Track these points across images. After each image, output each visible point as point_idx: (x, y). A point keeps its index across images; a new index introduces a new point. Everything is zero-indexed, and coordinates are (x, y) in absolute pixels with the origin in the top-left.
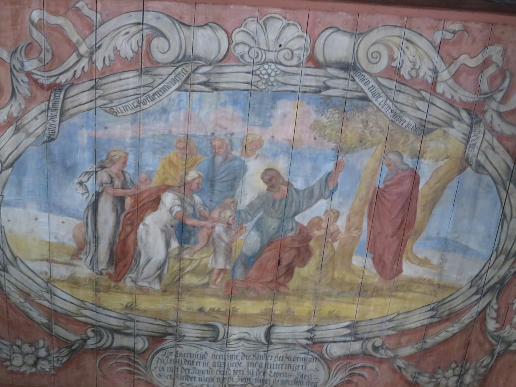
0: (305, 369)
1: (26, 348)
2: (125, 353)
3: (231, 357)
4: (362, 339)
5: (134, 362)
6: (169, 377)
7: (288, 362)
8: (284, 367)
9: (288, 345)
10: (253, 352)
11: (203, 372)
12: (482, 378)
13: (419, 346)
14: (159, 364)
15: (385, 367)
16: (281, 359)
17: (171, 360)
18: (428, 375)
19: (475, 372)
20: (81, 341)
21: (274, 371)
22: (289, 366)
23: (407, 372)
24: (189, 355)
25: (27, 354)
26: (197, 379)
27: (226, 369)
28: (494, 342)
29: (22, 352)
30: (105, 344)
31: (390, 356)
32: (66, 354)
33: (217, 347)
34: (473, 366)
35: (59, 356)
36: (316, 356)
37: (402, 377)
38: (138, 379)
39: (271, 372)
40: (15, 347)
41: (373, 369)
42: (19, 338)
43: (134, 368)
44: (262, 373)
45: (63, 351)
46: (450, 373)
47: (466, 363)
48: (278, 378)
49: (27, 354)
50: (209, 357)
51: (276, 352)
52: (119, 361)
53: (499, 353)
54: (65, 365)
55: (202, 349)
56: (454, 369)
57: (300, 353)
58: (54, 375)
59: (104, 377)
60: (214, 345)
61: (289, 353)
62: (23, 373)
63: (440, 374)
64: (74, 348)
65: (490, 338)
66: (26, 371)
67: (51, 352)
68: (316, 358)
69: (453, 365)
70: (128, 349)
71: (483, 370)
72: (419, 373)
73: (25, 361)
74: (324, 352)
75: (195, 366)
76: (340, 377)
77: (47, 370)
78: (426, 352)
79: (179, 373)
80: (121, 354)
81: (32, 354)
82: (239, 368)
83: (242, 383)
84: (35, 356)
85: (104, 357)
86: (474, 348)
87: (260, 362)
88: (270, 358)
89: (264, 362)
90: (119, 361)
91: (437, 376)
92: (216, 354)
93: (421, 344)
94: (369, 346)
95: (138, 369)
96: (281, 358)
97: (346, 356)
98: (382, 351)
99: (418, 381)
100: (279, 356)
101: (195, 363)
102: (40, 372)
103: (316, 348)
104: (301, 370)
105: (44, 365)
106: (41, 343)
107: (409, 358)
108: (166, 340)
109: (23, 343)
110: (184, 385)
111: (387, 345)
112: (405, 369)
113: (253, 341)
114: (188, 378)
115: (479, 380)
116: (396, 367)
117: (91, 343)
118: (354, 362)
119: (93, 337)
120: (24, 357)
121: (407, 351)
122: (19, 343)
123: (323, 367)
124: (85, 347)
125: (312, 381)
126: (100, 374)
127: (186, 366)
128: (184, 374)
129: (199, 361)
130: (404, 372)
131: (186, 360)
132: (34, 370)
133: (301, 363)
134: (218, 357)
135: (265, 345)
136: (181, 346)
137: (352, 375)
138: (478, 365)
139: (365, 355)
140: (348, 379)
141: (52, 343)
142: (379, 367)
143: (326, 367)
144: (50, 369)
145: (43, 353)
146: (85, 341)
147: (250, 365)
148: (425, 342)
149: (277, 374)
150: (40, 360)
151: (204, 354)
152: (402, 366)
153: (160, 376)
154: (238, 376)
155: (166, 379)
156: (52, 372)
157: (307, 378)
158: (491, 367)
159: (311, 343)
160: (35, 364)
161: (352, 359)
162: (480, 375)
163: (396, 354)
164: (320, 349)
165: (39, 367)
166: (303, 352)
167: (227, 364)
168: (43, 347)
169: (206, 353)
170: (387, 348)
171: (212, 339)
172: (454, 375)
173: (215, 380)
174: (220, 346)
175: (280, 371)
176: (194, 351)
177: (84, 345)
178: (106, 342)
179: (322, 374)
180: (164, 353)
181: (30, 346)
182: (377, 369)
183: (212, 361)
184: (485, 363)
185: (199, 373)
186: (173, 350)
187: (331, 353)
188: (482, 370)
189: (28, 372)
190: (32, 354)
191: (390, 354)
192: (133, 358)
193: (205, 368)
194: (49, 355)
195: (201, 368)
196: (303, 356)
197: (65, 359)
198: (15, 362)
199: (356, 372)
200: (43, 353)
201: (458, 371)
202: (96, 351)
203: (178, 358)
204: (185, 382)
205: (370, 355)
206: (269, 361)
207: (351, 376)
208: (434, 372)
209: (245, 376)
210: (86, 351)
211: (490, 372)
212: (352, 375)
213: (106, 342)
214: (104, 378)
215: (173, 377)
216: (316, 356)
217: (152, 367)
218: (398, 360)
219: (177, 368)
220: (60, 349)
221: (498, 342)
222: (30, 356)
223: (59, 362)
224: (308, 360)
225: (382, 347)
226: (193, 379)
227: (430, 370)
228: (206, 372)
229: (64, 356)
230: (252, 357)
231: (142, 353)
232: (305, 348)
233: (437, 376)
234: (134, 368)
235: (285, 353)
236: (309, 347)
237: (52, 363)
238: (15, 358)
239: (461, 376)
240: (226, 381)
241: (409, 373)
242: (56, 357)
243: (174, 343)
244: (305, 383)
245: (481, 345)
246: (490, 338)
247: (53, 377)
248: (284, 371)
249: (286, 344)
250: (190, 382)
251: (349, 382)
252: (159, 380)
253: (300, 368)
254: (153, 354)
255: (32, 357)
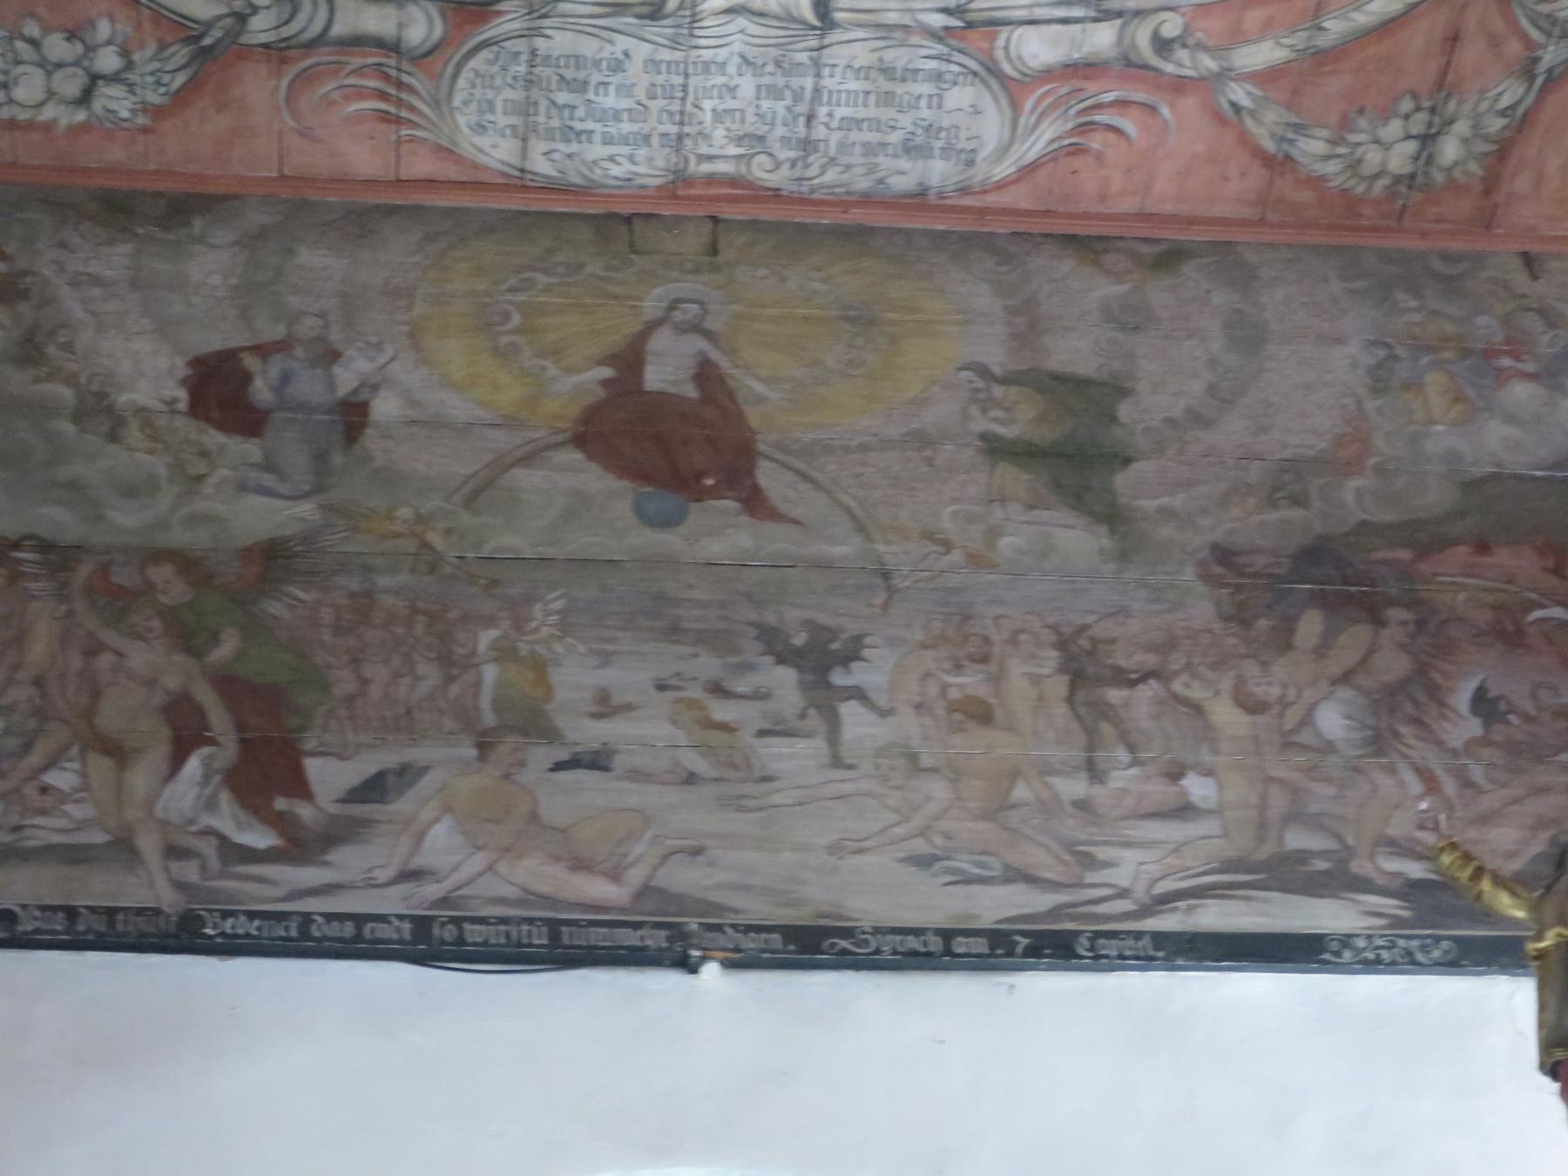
0: (940, 107)
1: (57, 47)
2: (371, 55)
3: (707, 65)
4: (1119, 14)
5: (400, 85)
6: (508, 131)
7: (886, 86)
8: (872, 99)
9: (886, 31)
10: (774, 52)
11: (617, 116)
12: (1495, 147)
13: (1299, 39)
14: (478, 92)
15: (1190, 103)
16: (862, 75)
17: (515, 78)
18: (1325, 133)
19: (1474, 127)
20: (229, 21)
21: (841, 112)
22: (887, 99)
23: (1259, 122)
24: (572, 61)
25: (60, 66)
26: (597, 138)
27: (689, 107)
28: (1535, 34)
29: (44, 58)
30: (303, 30)
31: (1209, 70)
32: (183, 61)
33: (660, 35)
34: (1467, 107)
35: (159, 70)
36: (973, 65)
37: (1244, 139)
38: (412, 139)
39: (830, 115)
40: (19, 44)
41: (1152, 109)
42: (33, 15)
43: (400, 103)
44: (802, 120)
45: (173, 55)
46: (1394, 128)
47: (1449, 96)
48: (855, 136)
49: (60, 66)
50: (635, 68)
51: (845, 51)
52: (352, 81)
53: (1550, 71)
54: (181, 98)
55: (611, 42)
56: (1407, 117)
57: (921, 56)
58: (144, 130)
59: (305, 133)
60: (652, 30)
61: (889, 55)
62: (48, 127)
63: (1363, 131)
64: (207, 41)
65: (1524, 23)
66: (55, 121)
67: (136, 57)
68: (975, 74)
69: (1407, 105)
70: (379, 43)
71: (1500, 123)
72: (1298, 128)
73: (55, 87)
74: (999, 54)
75: (590, 95)
76: (1048, 136)
77: (125, 114)
78: (1321, 60)
79: (541, 119)
80: (358, 61)
81: (76, 64)
82: (731, 104)
83: (741, 151)
84: (85, 69)
85: (306, 70)
86: (1472, 53)
87: (795, 82)
88: (826, 71)
89: (809, 83)
90: (352, 81)
91: (1353, 138)
92: (658, 57)
93: (1305, 34)
94: (1142, 37)
95: (412, 108)
96: (863, 72)
97: (1067, 66)
98: (1182, 55)
99: (1295, 153)
100: (857, 65)
101: (592, 88)
102: (101, 121)
103: (976, 40)
104: (925, 113)
105: (115, 101)
106: (104, 29)
107: (1266, 78)
108: (499, 13)
109: (47, 30)
110: (556, 156)
111: (1199, 35)
112: (1252, 113)
113: (776, 17)
114: (569, 134)
115: (1486, 154)
116: (1225, 105)
117: (261, 28)
118: (1091, 87)
119: (267, 8)
120: (49, 74)
121: (1261, 54)
122: (32, 29)
123: (996, 99)
124: (244, 39)
125: (959, 147)
126: (292, 124)
127: (562, 98)
128: (555, 123)
129: (606, 80)
130: (1249, 123)
131: (562, 77)
132: (81, 116)
133: (924, 88)
134: (664, 68)
135: (814, 28)
136: (548, 32)
137: (1086, 128)
138: (1484, 106)
139: (1129, 65)
140: (1074, 140)
141: (138, 27)
142: (1172, 106)
143: (1004, 102)
144: (133, 111)
145: (108, 61)
146: (242, 18)
147: (763, 94)
148: (1321, 29)
149: (850, 123)
150: (101, 83)
151: (621, 57)
152: (1245, 102)
153: (481, 128)
154: (728, 129)
155: (499, 140)
156: (141, 120)
157: (943, 134)
158: (1525, 115)
159: (960, 24)
160: (85, 99)
161: (1086, 78)
162: (1487, 139)
163: (1226, 65)
164: (986, 45)
165: (98, 105)
166: (933, 52)
167: (691, 89)
168: (109, 43)
169: (627, 54)
170: (1200, 46)
171: (646, 10)
172: (1409, 137)
173: (655, 141)
174: (669, 31)
175: (861, 113)
176: (588, 47)
177: (239, 33)
178: (311, 20)
179: (991, 125)
180: (491, 56)
181: (68, 39)
182: (1165, 111)
183: (643, 81)
184: (1505, 101)
185: (603, 116)
186: (519, 45)
187: (1020, 58)
188: (1496, 124)
189: (63, 122)
190: (76, 64)
191: (1209, 63)
192: (393, 73)
193: (625, 103)
194: (130, 66)
195: (610, 101)
196: (932, 65)
197: (180, 79)
198: (20, 93)
199: (1097, 118)
200: (108, 61)
201: (1419, 123)
202: (279, 52)
203: (536, 71)
204: (561, 147)
205: (1146, 67)
206: (827, 82)
207: (1081, 133)
208: (1345, 124)
209: (748, 129)
210: (246, 53)
211: (1519, 130)
212: (1086, 128)
213: (311, 20)
214: (304, 135)
215: (520, 130)
216: (973, 65)
217: (457, 102)
218: (1233, 85)
219: (536, 103)
220: (163, 46)
221: (1548, 34)
222: (70, 70)
223: (162, 90)
224: (948, 77)
225: (1181, 41)
226: (584, 138)
227: (1333, 118)
228: (625, 116)
229: (178, 70)
230: (770, 68)
231: (425, 56)
232: (940, 39)
233: (1353, 138)
234: (400, 103)
235: (876, 56)
236: (954, 37)
237: (139, 91)
238: (21, 80)
239: (1428, 139)
240: (688, 143)
241: (1265, 129)
242: (152, 74)
243: (525, 25)
244: (937, 153)
245: (1494, 42)
246: (1524, 23)
247: (141, 138)
248: (872, 112)
249: (879, 26)
250: (574, 147)
251: (1076, 150)
252: (479, 141)
253: (923, 102)
254: (457, 58)
255: (74, 75)
